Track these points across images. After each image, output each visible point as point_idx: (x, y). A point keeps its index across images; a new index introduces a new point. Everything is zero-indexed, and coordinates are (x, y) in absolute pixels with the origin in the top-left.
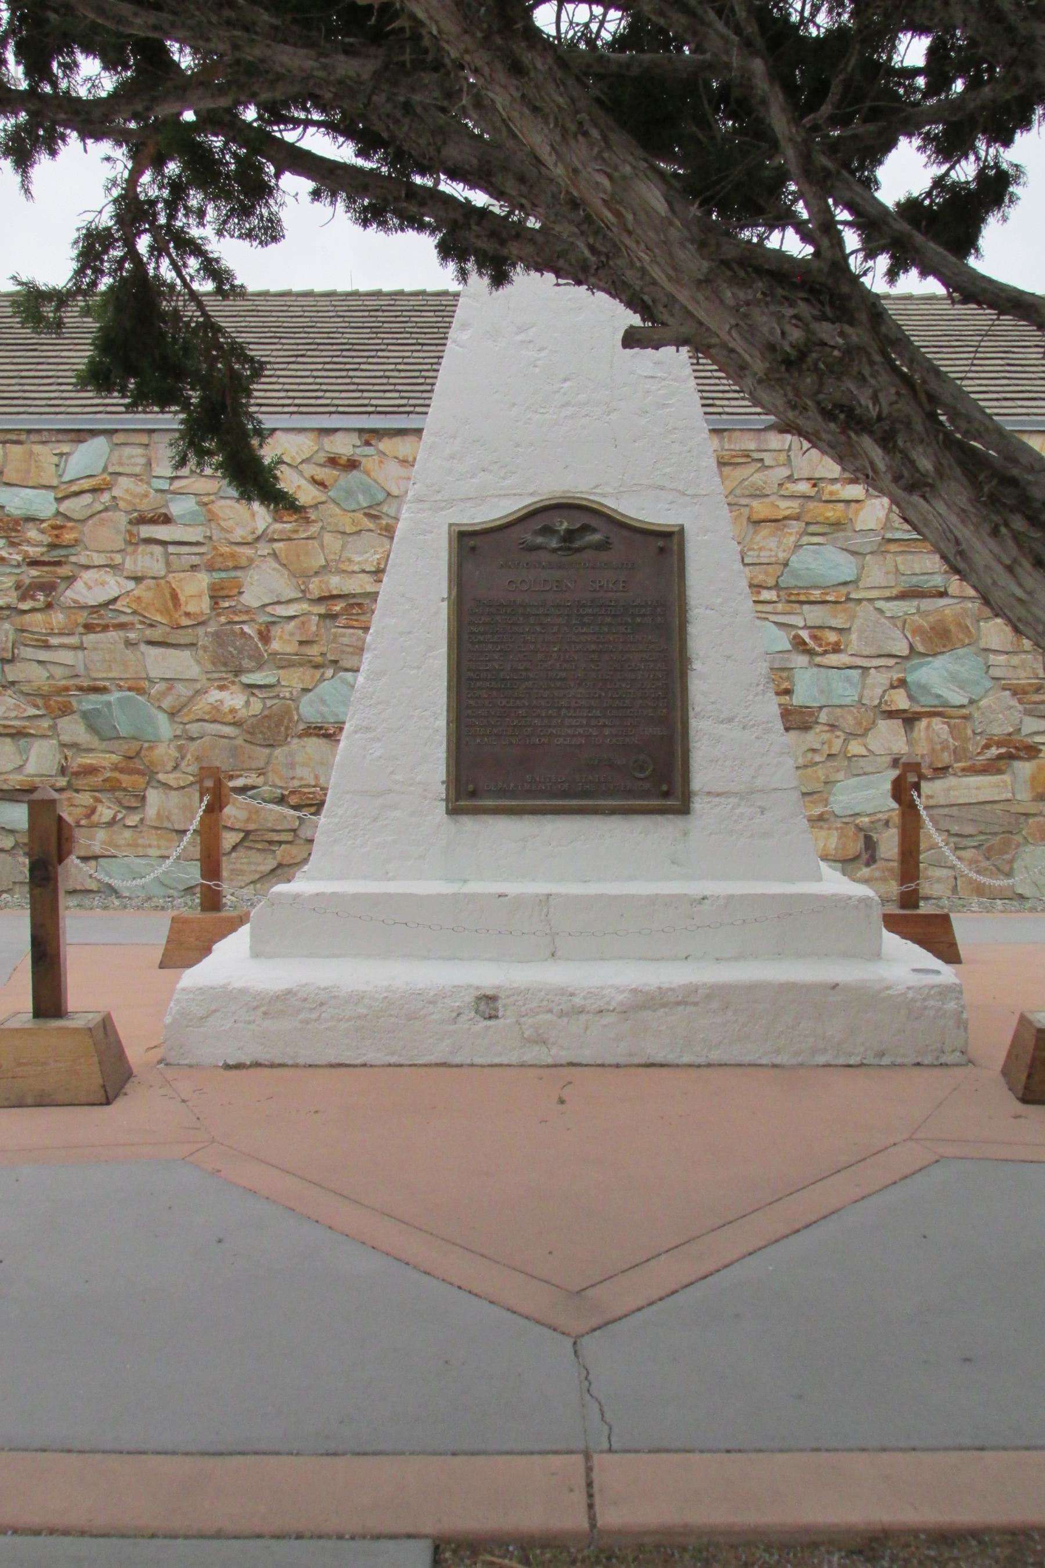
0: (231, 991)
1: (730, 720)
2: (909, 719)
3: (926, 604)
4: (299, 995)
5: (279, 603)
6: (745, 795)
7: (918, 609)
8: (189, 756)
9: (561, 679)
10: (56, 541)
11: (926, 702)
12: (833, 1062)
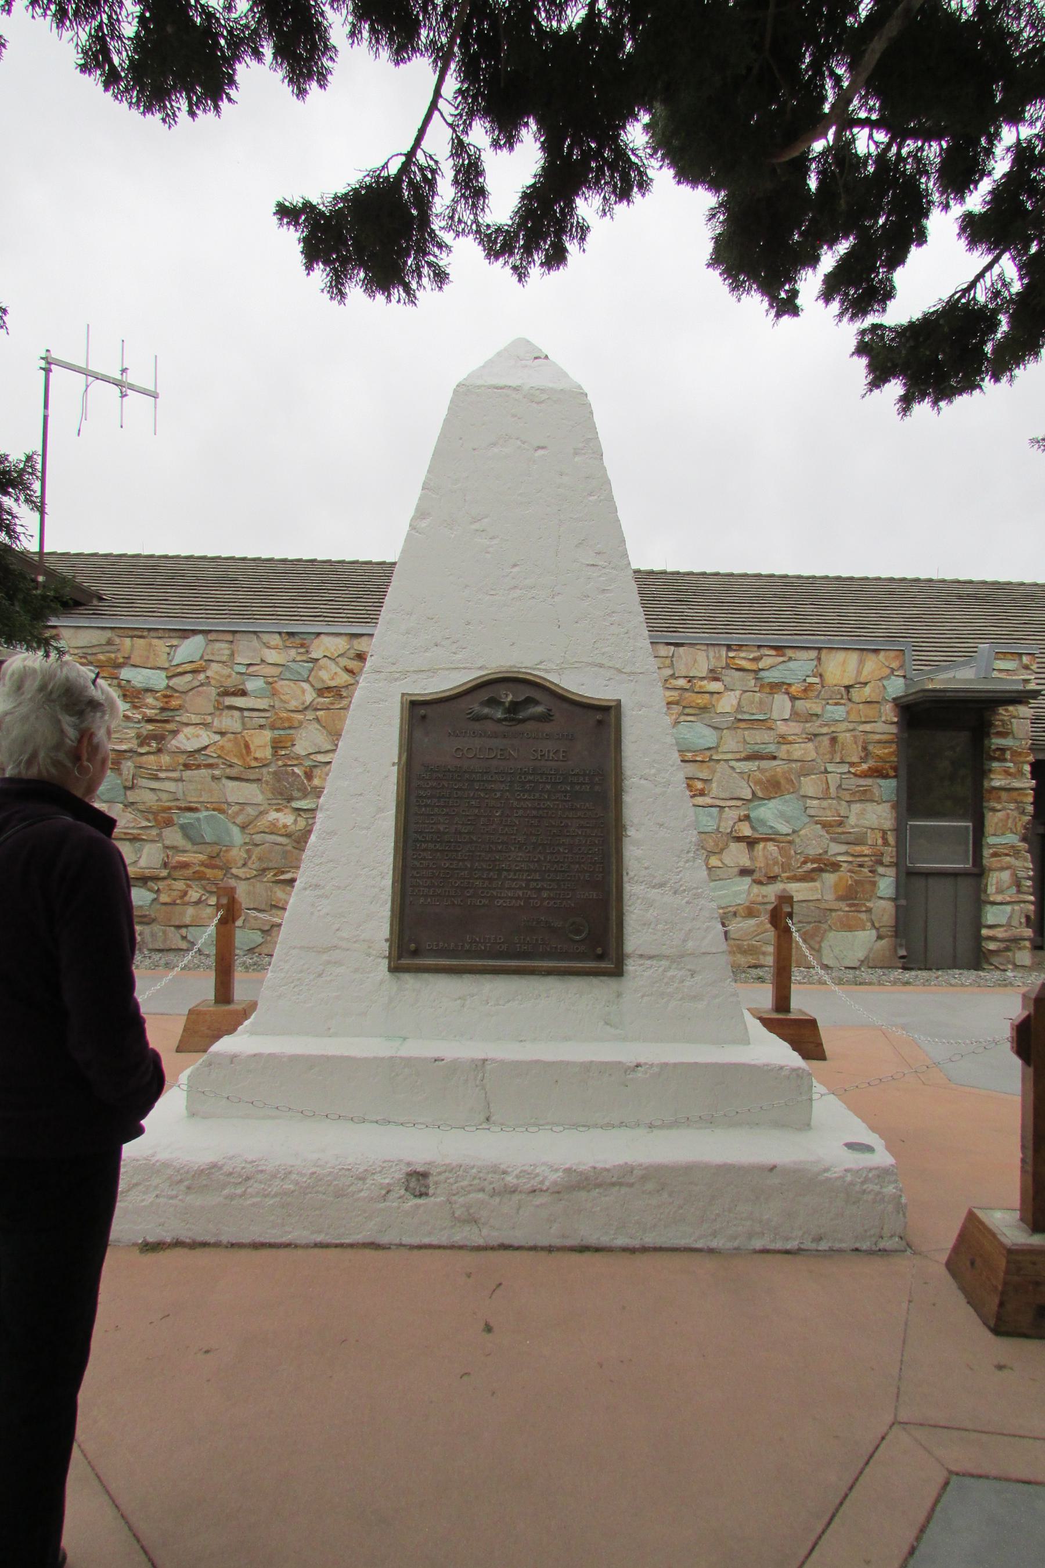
0: (154, 1165)
1: (662, 885)
2: (751, 843)
3: (765, 764)
4: (225, 1169)
5: (319, 752)
6: (678, 958)
7: (759, 767)
8: (254, 857)
9: (502, 843)
10: (166, 706)
12: (772, 1246)
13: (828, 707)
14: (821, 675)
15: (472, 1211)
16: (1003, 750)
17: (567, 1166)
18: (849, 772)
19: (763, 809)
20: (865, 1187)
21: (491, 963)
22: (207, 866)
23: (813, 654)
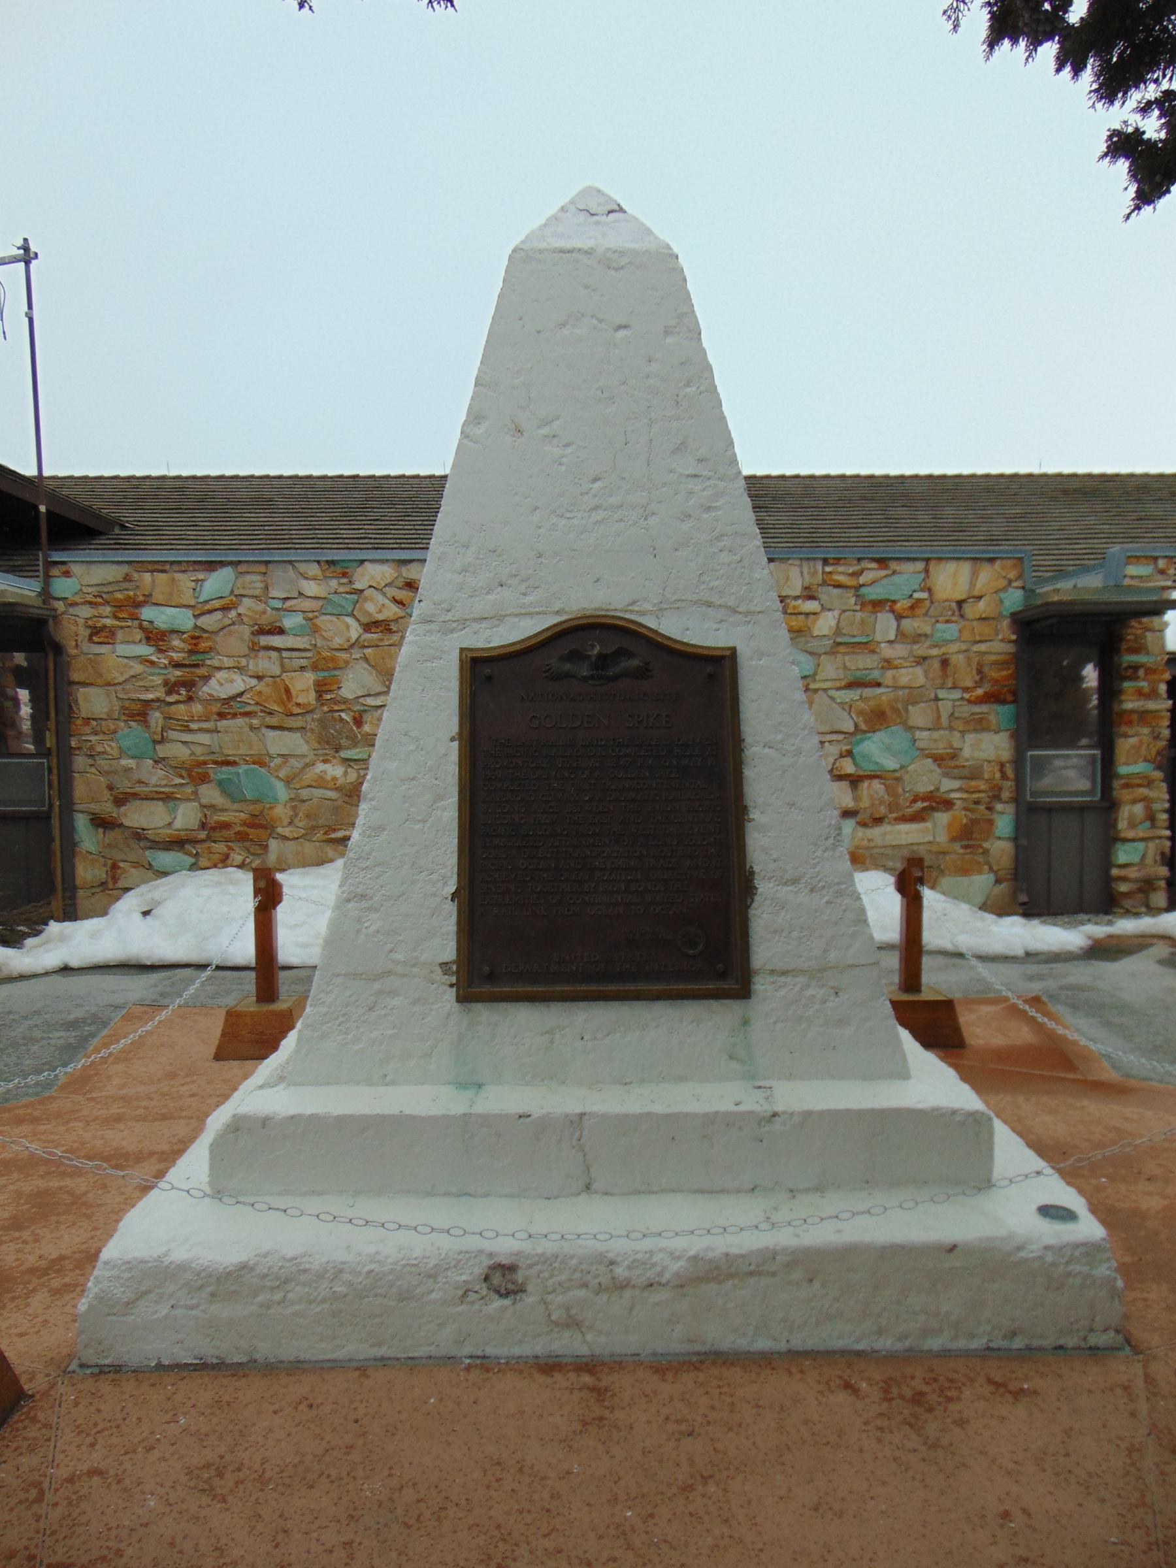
0: (167, 1267)
2: (854, 781)
3: (868, 692)
8: (301, 814)
11: (867, 768)
13: (939, 626)
14: (929, 590)
15: (573, 1312)
16: (1136, 667)
17: (692, 1253)
18: (962, 698)
19: (866, 742)
20: (1070, 1268)
21: (584, 987)
22: (250, 826)
23: (920, 566)
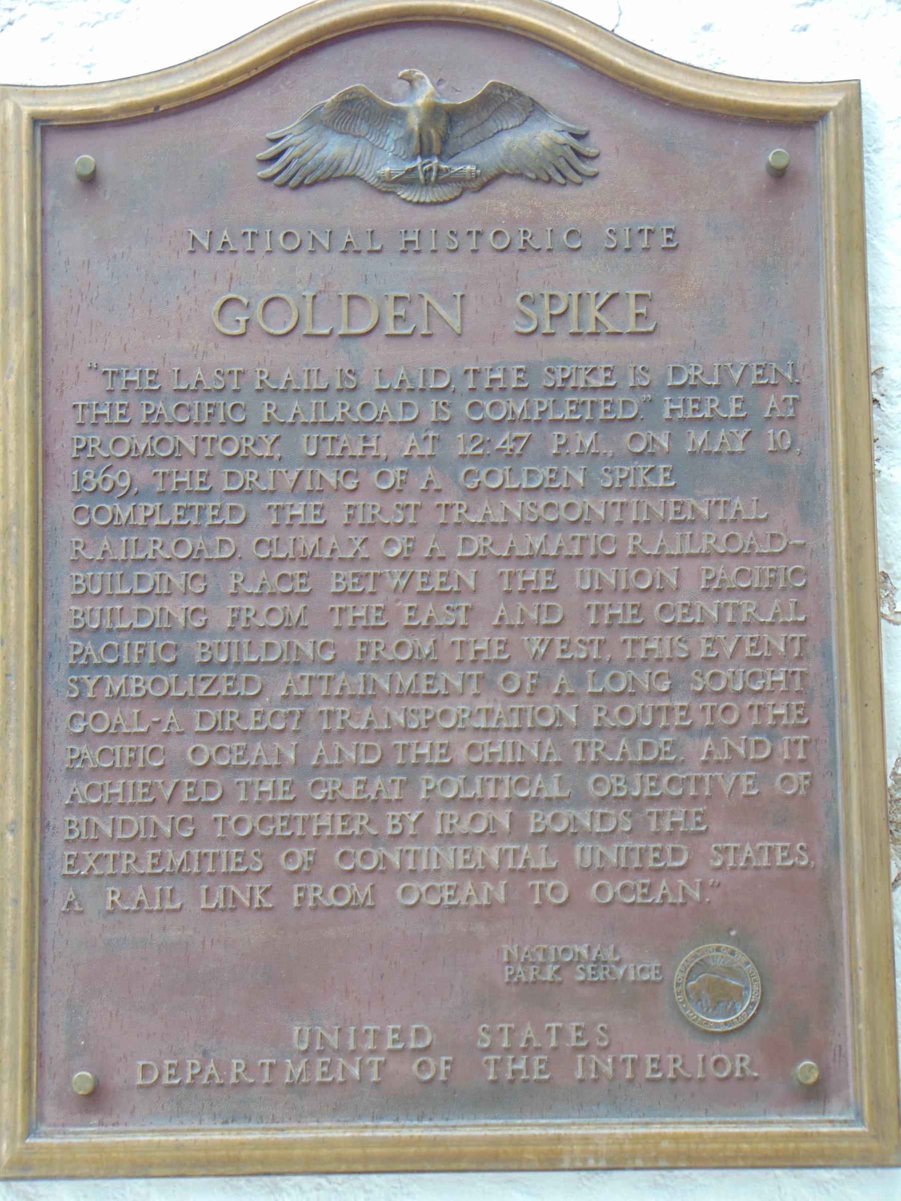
21: (389, 1131)
